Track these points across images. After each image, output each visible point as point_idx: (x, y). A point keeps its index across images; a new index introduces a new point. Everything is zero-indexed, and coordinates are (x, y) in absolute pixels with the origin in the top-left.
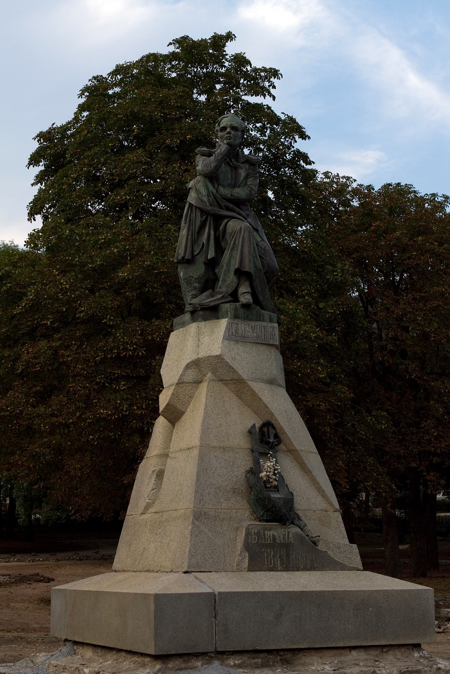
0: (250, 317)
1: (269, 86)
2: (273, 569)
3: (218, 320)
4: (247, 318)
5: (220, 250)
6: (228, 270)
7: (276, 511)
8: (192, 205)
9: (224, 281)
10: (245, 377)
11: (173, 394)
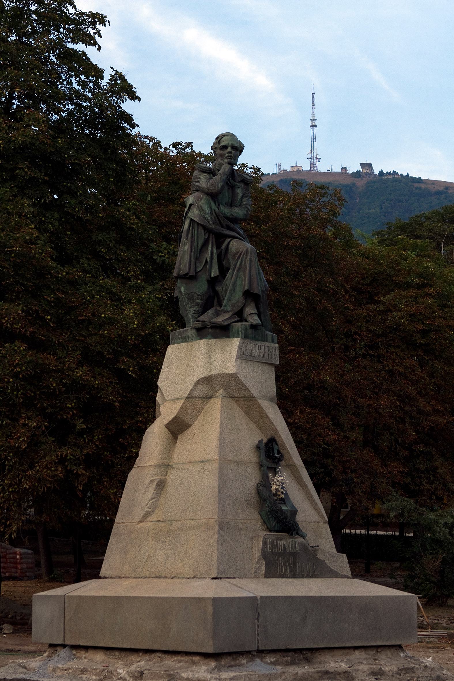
0: (257, 337)
1: (95, 33)
2: (283, 576)
3: (229, 339)
4: (254, 339)
5: (223, 271)
6: (234, 290)
7: (286, 522)
8: (194, 221)
9: (229, 300)
10: (255, 395)
11: (182, 408)
